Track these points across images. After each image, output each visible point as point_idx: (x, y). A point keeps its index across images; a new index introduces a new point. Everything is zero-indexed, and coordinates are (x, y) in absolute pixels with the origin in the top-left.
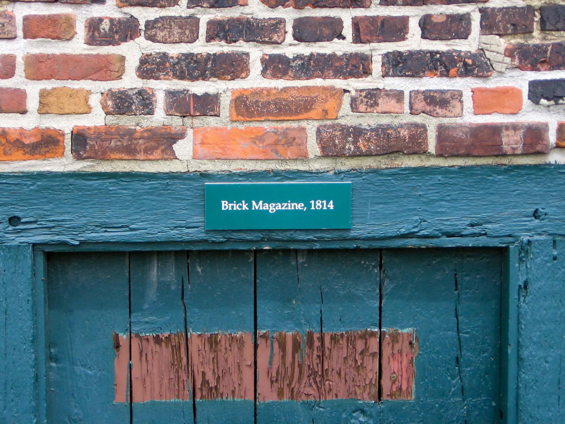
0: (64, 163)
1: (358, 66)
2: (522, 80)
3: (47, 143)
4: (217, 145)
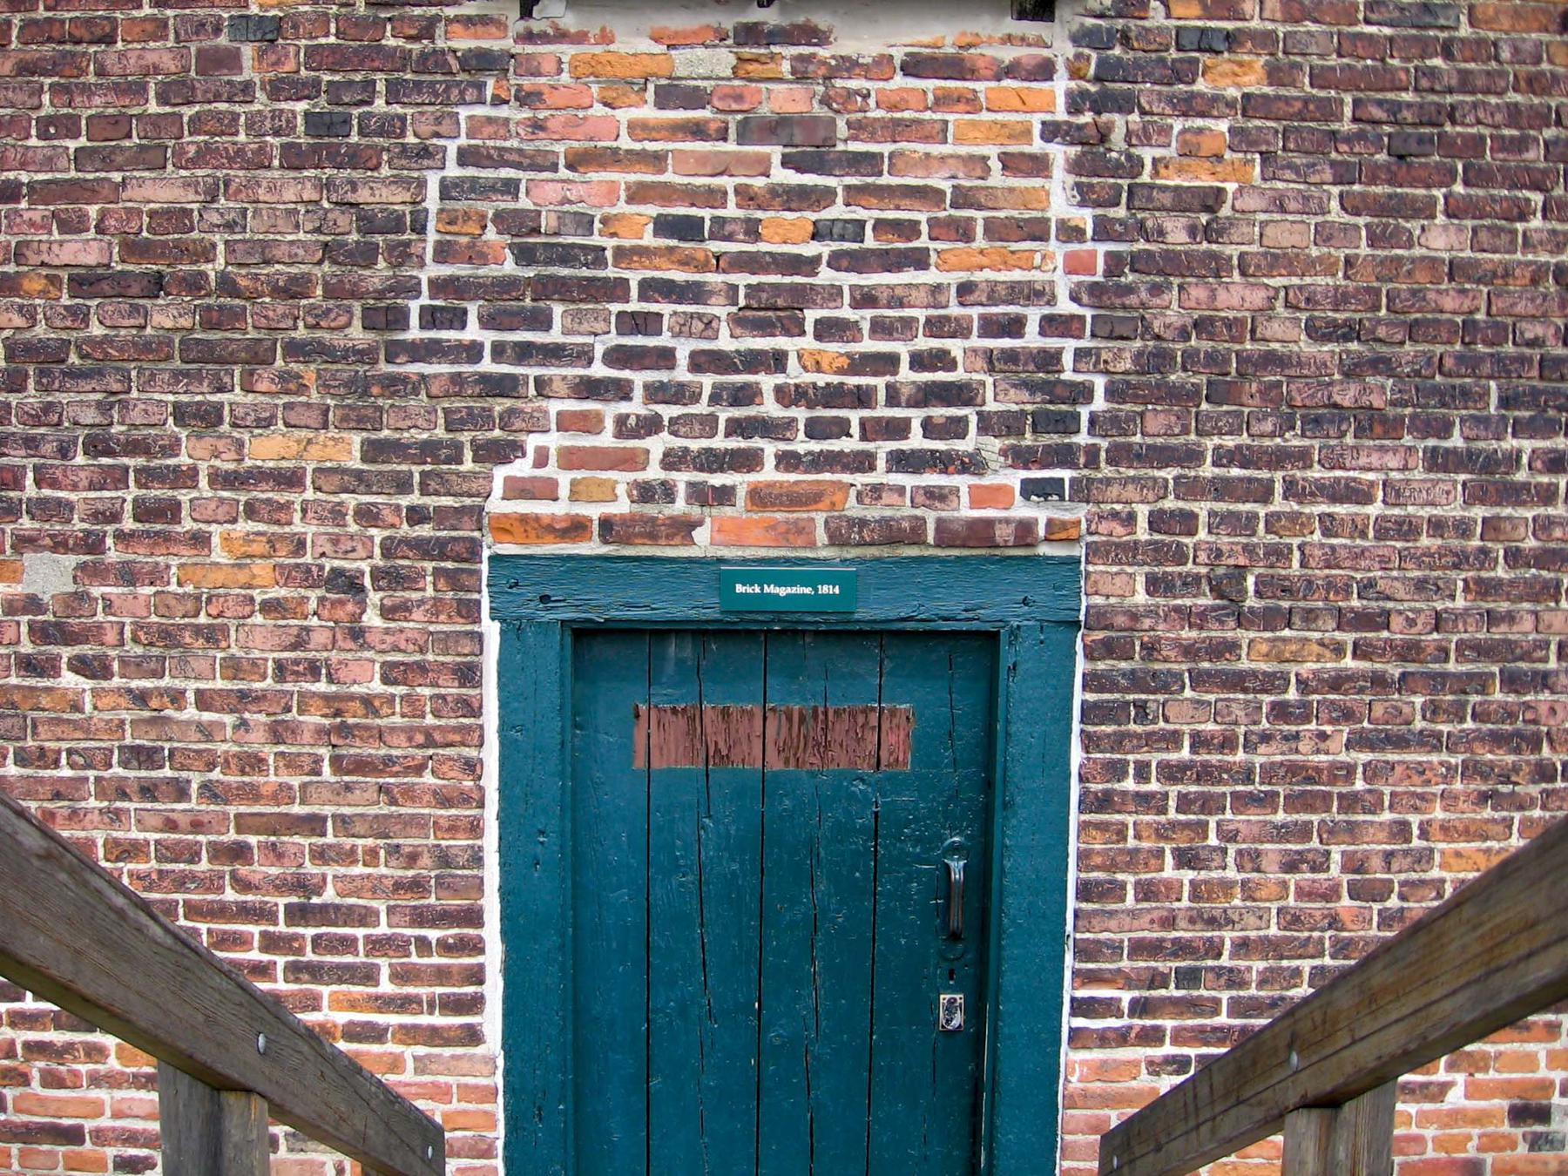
0: (591, 547)
1: (863, 462)
2: (1014, 478)
3: (577, 528)
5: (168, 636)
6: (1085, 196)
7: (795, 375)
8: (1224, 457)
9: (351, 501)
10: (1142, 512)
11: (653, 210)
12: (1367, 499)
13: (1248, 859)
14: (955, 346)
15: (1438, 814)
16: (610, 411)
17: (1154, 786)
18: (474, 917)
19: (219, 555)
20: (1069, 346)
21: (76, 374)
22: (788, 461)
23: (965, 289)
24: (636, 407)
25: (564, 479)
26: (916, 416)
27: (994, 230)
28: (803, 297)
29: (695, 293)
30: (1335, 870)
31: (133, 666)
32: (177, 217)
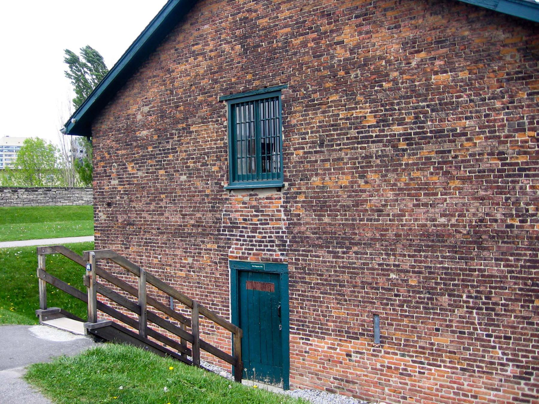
0: (238, 260)
1: (264, 250)
2: (279, 253)
3: (236, 257)
4: (251, 259)
5: (200, 268)
6: (285, 215)
7: (256, 239)
8: (303, 251)
9: (216, 253)
10: (294, 258)
11: (242, 218)
12: (320, 258)
13: (309, 309)
14: (272, 235)
15: (332, 305)
16: (239, 243)
17: (297, 297)
18: (228, 307)
19: (205, 259)
20: (285, 235)
21: (192, 236)
22: (257, 250)
23: (273, 228)
24: (242, 242)
25: (235, 251)
26: (269, 244)
27: (276, 220)
28: (257, 228)
29: (246, 228)
30: (319, 312)
31: (198, 272)
32: (200, 218)
